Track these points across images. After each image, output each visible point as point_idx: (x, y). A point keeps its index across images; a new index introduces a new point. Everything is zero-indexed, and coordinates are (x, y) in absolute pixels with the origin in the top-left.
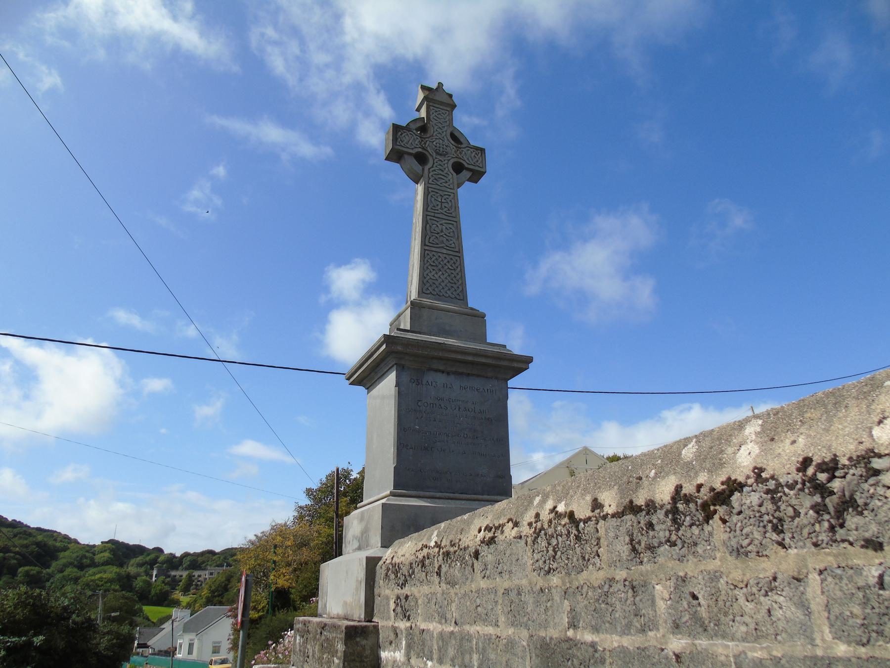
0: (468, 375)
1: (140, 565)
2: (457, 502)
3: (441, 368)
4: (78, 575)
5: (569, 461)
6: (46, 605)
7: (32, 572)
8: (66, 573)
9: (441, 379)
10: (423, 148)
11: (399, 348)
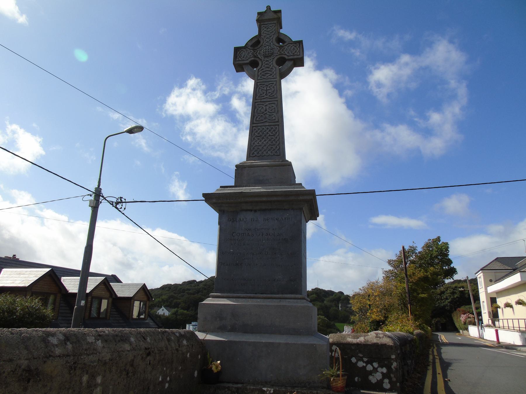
0: (271, 210)
2: (254, 300)
9: (249, 216)
10: (255, 57)
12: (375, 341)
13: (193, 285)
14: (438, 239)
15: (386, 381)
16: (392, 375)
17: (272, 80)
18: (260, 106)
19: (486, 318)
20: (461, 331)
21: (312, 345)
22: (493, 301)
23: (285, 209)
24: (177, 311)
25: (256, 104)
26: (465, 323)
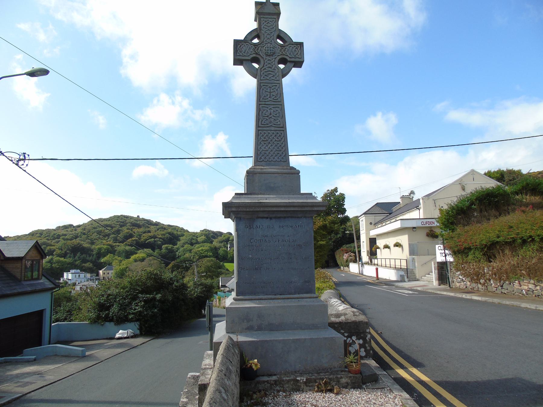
0: (285, 217)
1: (221, 242)
3: (265, 216)
4: (191, 248)
5: (461, 179)
6: (161, 278)
7: (169, 248)
8: (185, 247)
9: (266, 223)
10: (257, 54)
11: (234, 209)
12: (354, 319)
13: (69, 230)
14: (336, 190)
15: (363, 350)
16: (367, 345)
17: (275, 82)
18: (264, 108)
19: (365, 257)
20: (342, 268)
21: (332, 338)
22: (372, 242)
23: (298, 217)
24: (52, 259)
25: (261, 106)
26: (347, 261)
